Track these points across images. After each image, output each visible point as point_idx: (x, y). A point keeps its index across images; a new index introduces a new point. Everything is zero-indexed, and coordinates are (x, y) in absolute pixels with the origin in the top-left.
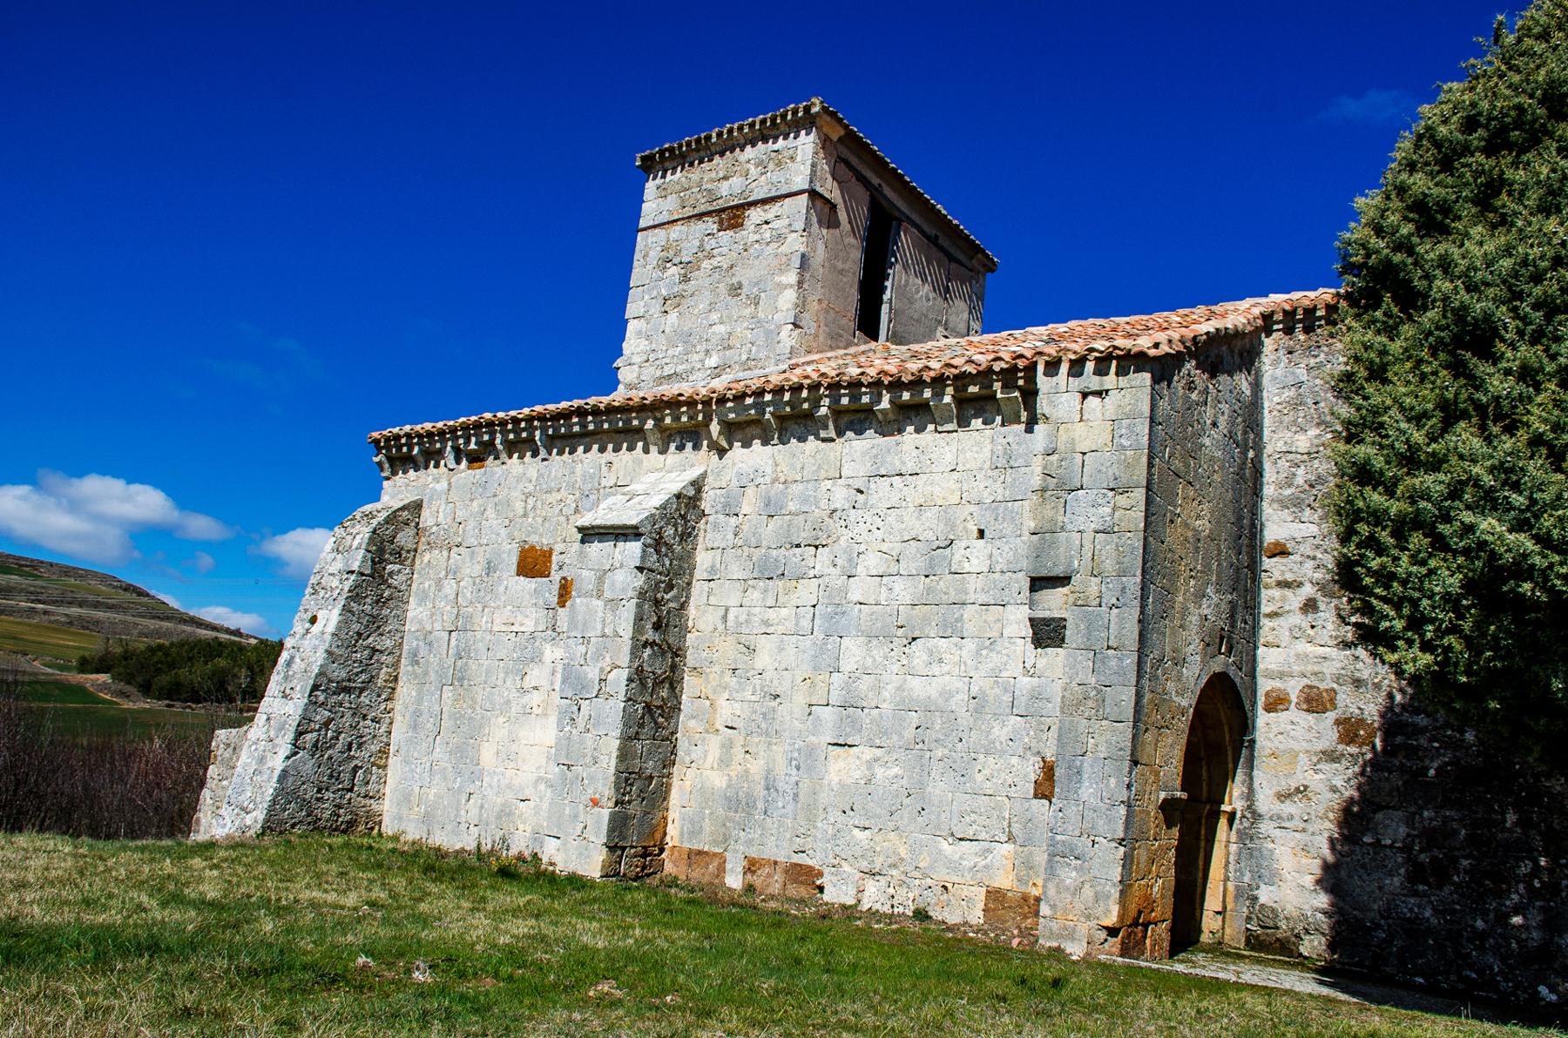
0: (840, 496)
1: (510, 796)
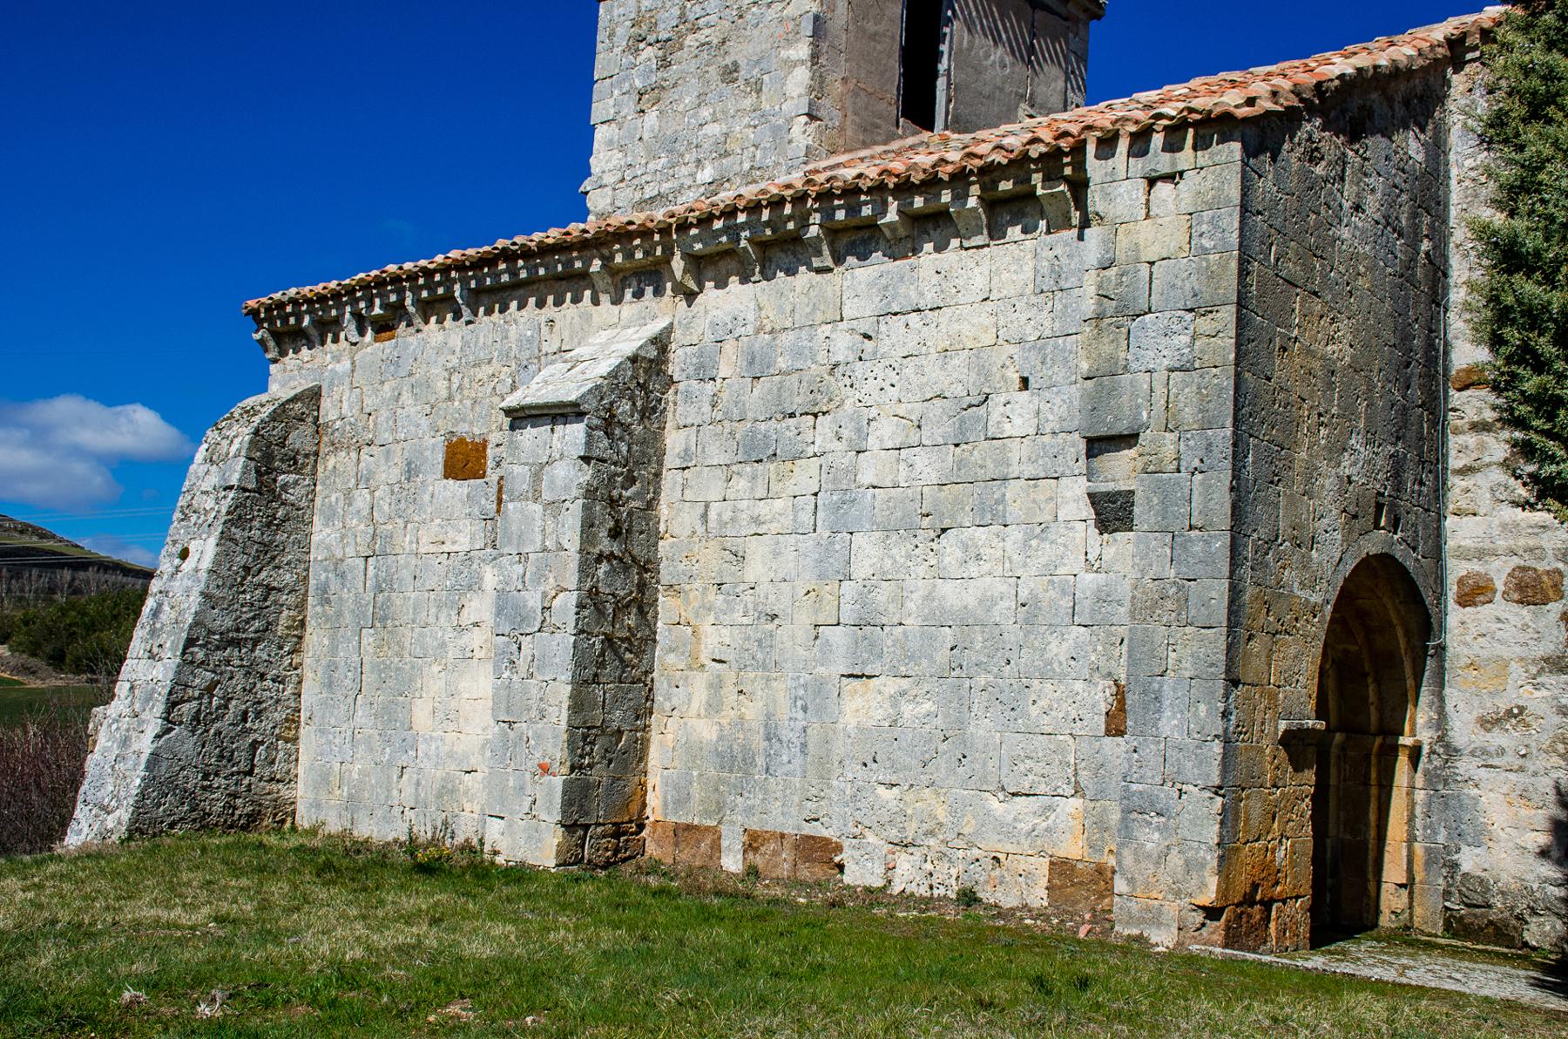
0: (843, 345)
1: (452, 767)
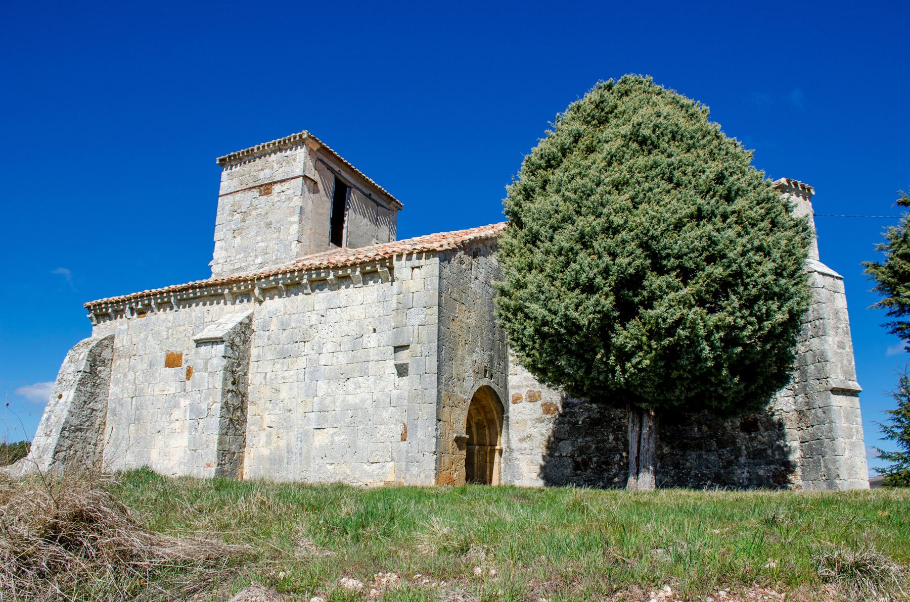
0: (314, 319)
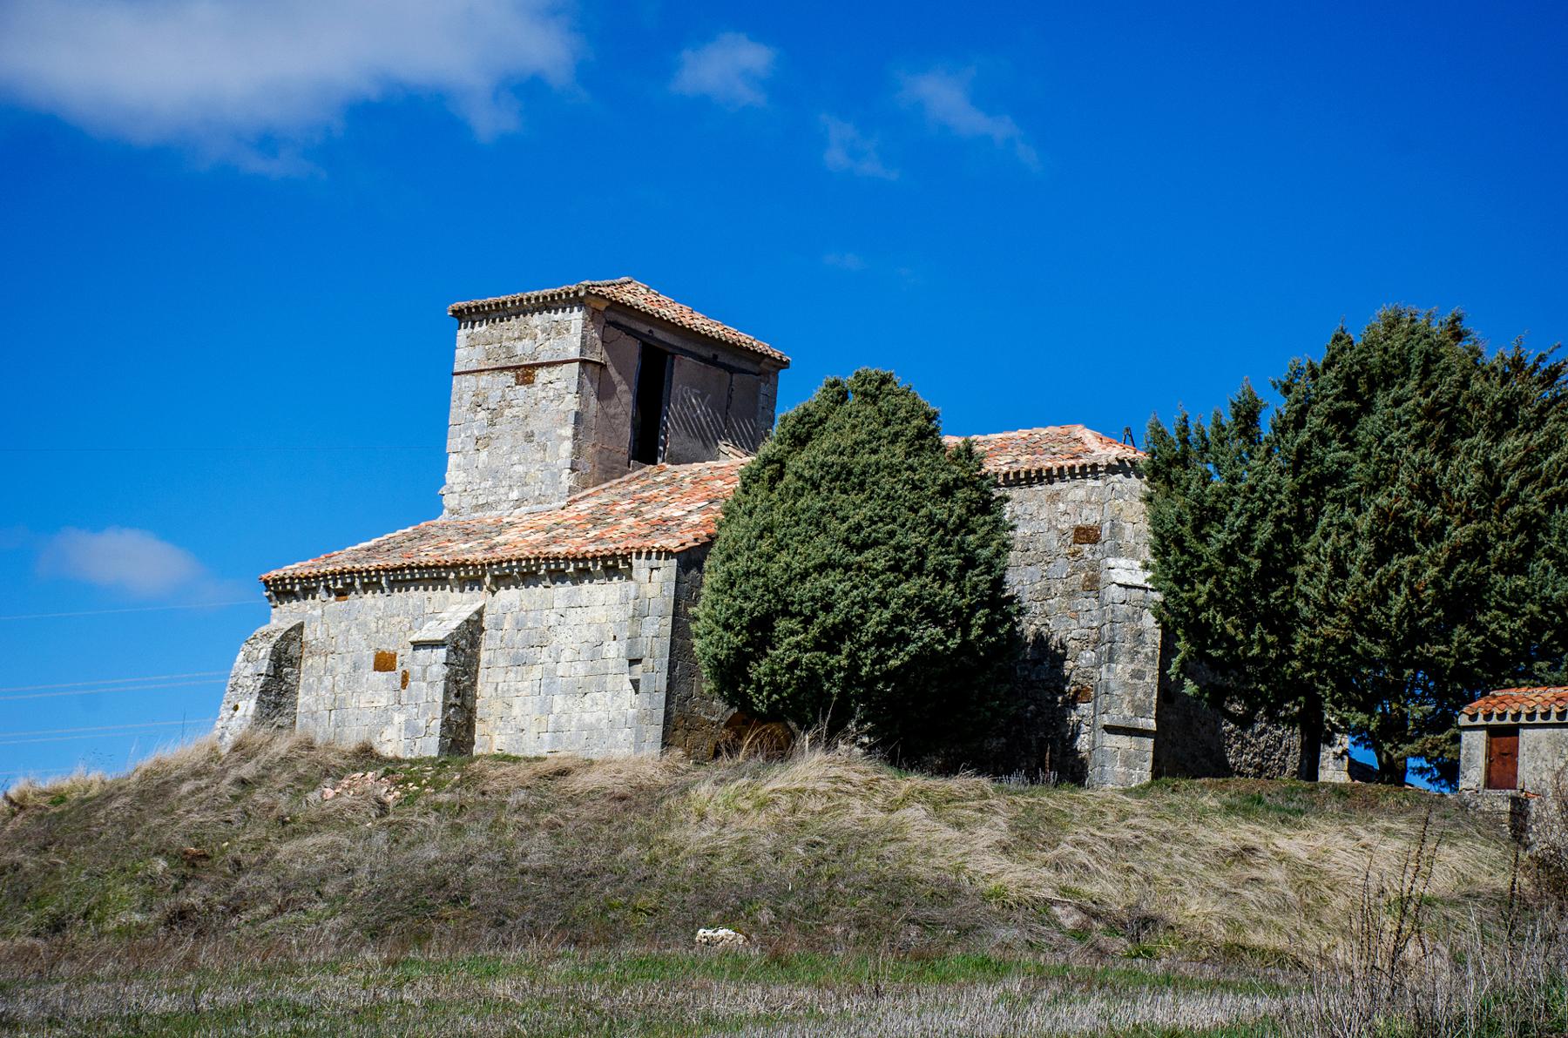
0: (553, 618)
